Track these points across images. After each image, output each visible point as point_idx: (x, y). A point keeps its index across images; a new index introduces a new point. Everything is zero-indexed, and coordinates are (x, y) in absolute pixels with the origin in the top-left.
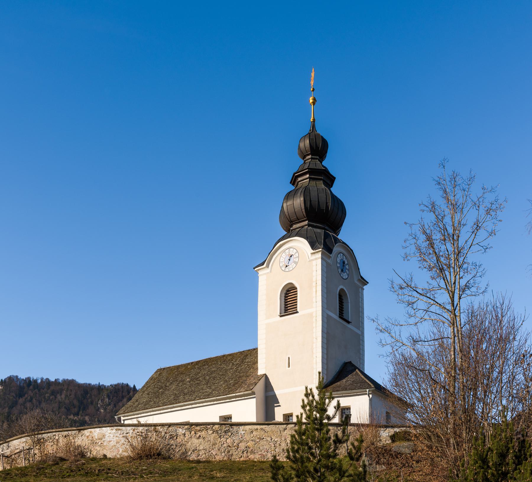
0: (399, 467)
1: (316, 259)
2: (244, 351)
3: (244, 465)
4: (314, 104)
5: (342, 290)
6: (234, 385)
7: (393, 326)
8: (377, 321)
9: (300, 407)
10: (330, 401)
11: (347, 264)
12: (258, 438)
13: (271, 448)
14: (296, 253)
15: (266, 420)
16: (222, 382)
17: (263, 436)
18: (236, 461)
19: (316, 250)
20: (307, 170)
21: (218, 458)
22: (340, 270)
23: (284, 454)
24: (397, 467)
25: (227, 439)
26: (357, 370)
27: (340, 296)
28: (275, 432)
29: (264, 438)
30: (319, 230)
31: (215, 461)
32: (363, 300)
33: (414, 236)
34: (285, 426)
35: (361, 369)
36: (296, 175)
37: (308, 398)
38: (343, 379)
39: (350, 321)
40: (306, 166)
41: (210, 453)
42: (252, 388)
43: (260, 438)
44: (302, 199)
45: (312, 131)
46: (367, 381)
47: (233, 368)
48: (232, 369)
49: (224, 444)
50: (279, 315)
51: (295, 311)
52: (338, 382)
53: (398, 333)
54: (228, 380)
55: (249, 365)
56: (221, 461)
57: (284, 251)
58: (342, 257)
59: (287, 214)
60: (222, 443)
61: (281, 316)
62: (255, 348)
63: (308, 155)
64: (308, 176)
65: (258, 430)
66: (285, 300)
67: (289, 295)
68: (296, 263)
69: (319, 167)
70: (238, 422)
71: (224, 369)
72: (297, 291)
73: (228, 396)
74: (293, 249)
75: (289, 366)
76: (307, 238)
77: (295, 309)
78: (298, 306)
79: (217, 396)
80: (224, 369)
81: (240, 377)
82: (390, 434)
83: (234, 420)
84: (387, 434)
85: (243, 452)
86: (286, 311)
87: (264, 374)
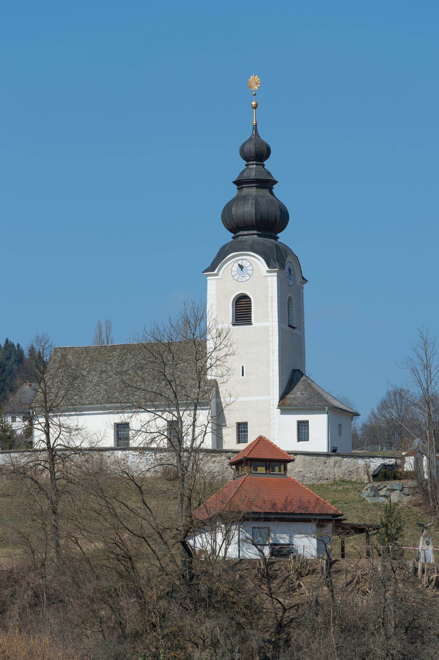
14: (249, 266)
15: (118, 446)
68: (250, 276)
75: (243, 375)
77: (237, 311)
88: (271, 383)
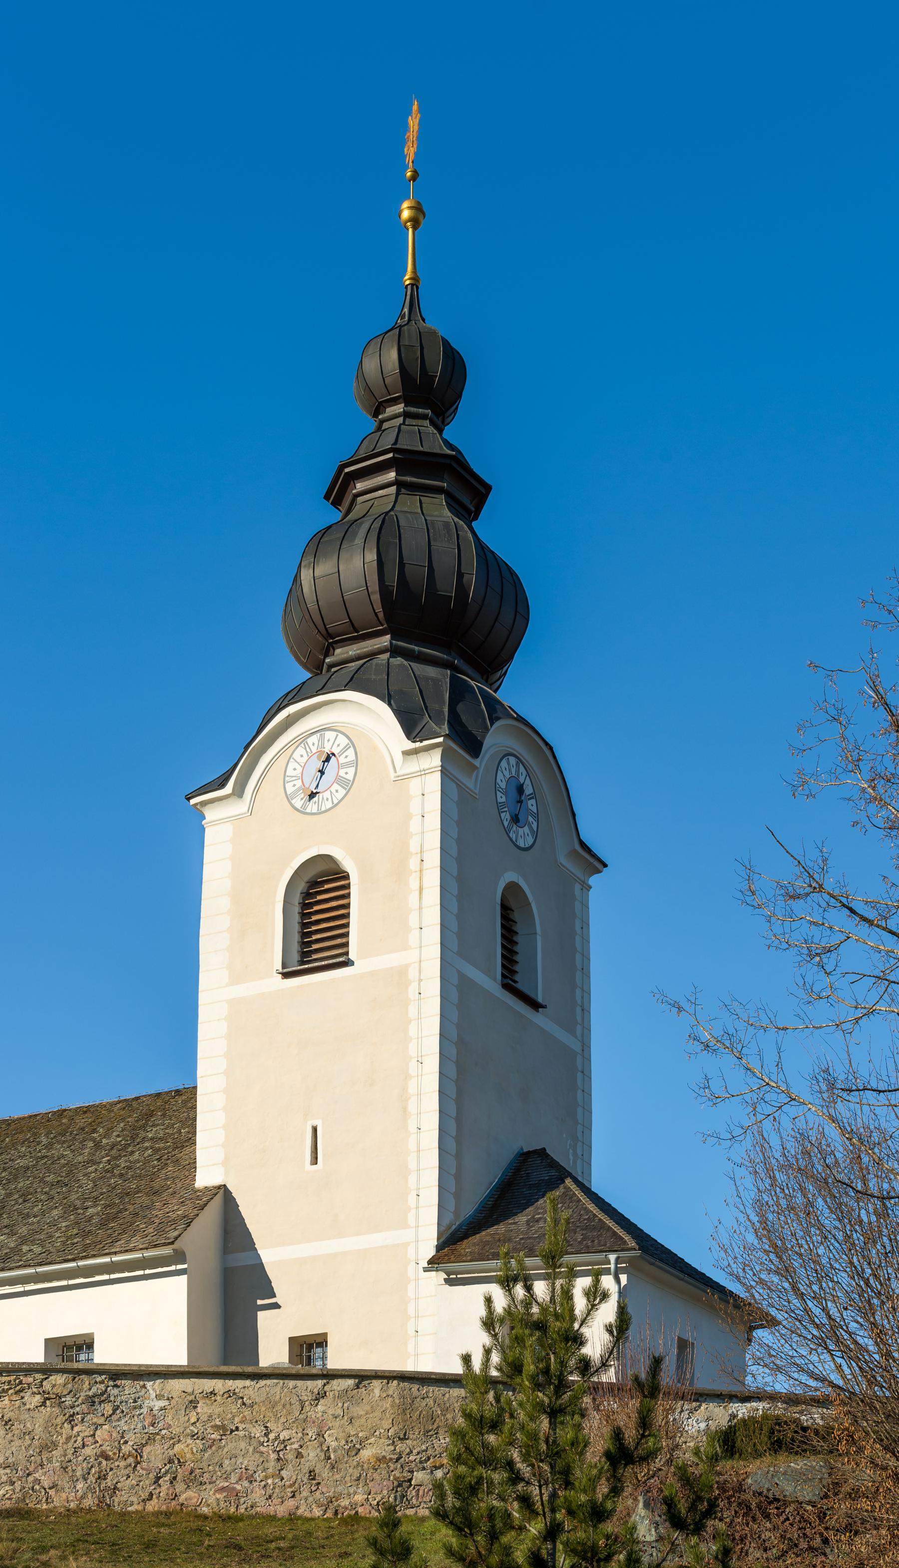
0: (774, 1551)
1: (423, 773)
2: (137, 1098)
3: (162, 1530)
4: (415, 222)
5: (512, 888)
6: (103, 1224)
7: (751, 1029)
8: (692, 1011)
9: (479, 1324)
10: (593, 1306)
11: (533, 796)
12: (216, 1427)
13: (266, 1465)
14: (346, 748)
16: (55, 1212)
17: (237, 1420)
18: (129, 1512)
19: (421, 741)
20: (391, 455)
21: (59, 1500)
22: (506, 816)
23: (314, 1488)
24: (765, 1550)
25: (97, 1426)
26: (568, 1182)
27: (505, 908)
28: (279, 1407)
29: (237, 1429)
30: (431, 671)
31: (50, 1511)
32: (585, 925)
33: (833, 712)
34: (320, 1383)
35: (580, 1179)
36: (347, 470)
37: (509, 1290)
38: (516, 1214)
39: (540, 1000)
40: (387, 441)
41: (30, 1479)
42: (176, 1238)
43: (223, 1427)
44: (372, 556)
45: (409, 320)
46: (610, 1223)
47: (96, 1158)
48: (94, 1163)
49: (84, 1446)
50: (281, 970)
51: (341, 959)
52: (497, 1222)
53: (771, 1058)
54: (78, 1203)
55: (159, 1149)
56: (75, 1512)
57: (302, 740)
58: (513, 770)
59: (312, 605)
60: (79, 1443)
61: (286, 975)
62: (181, 1087)
63: (394, 401)
64: (392, 475)
65: (218, 1398)
66: (303, 915)
67: (319, 898)
68: (348, 785)
69: (433, 443)
70: (140, 1366)
71: (62, 1161)
72: (348, 887)
73: (81, 1263)
74: (334, 734)
76: (388, 698)
78: (353, 939)
79: (40, 1264)
80: (62, 1161)
81: (127, 1194)
82: (713, 1426)
83: (103, 1355)
84: (703, 1426)
85: (158, 1478)
86: (305, 956)
87: (219, 1187)
88: (412, 1180)
